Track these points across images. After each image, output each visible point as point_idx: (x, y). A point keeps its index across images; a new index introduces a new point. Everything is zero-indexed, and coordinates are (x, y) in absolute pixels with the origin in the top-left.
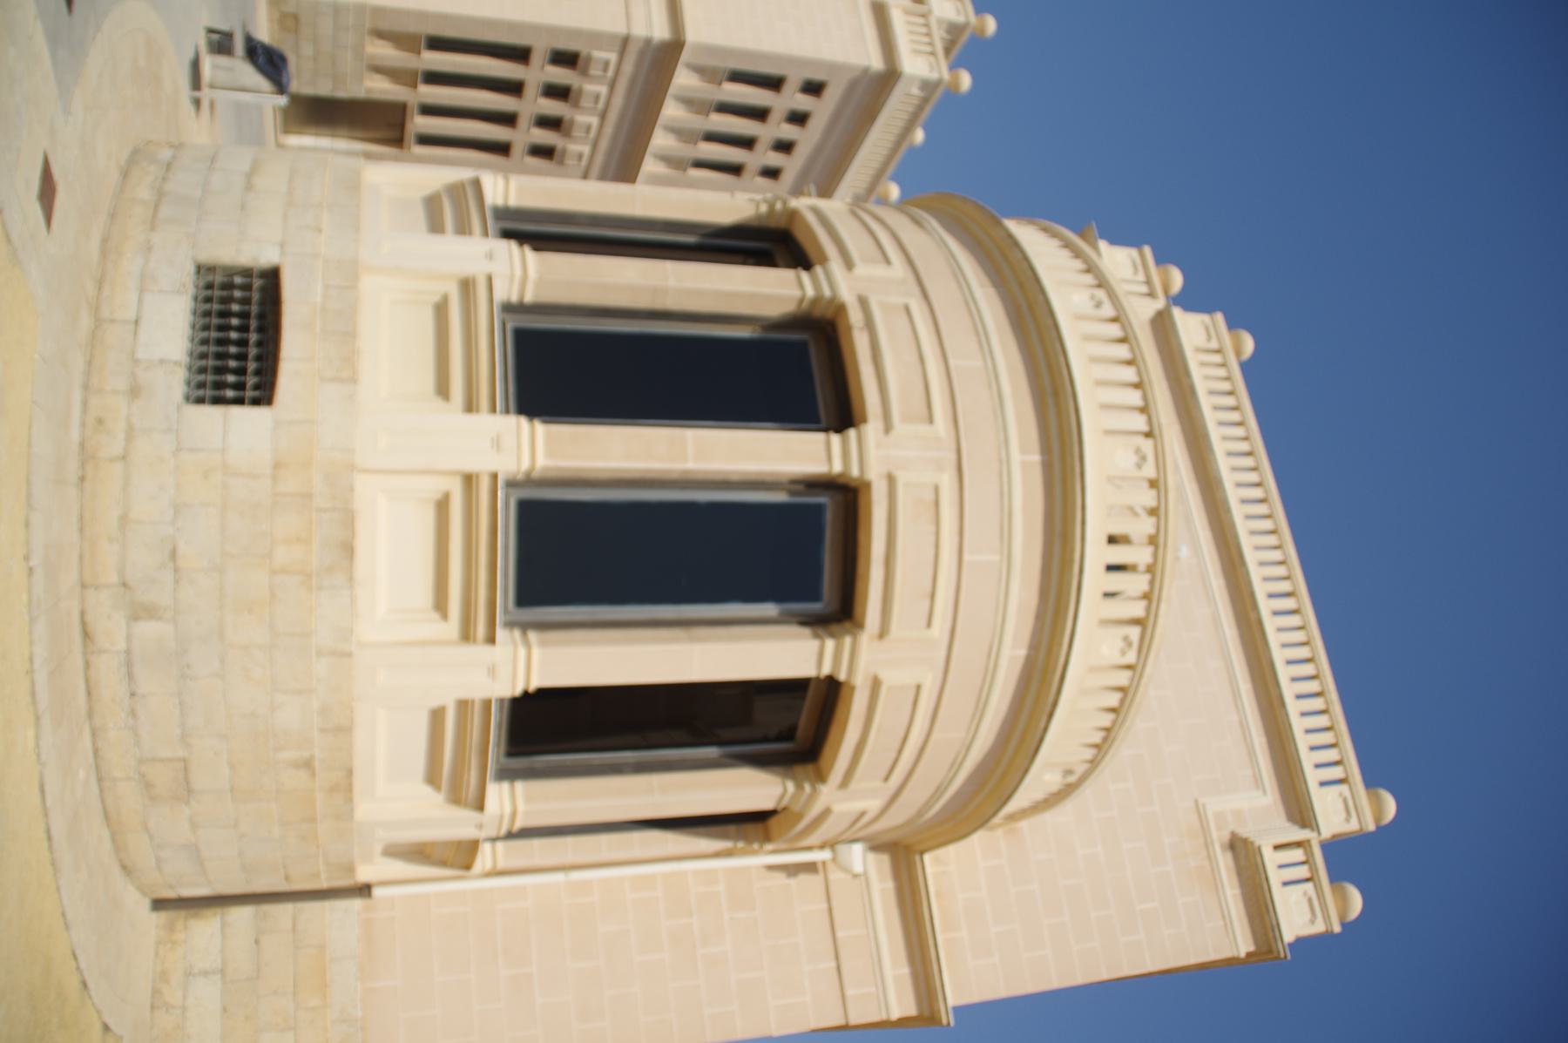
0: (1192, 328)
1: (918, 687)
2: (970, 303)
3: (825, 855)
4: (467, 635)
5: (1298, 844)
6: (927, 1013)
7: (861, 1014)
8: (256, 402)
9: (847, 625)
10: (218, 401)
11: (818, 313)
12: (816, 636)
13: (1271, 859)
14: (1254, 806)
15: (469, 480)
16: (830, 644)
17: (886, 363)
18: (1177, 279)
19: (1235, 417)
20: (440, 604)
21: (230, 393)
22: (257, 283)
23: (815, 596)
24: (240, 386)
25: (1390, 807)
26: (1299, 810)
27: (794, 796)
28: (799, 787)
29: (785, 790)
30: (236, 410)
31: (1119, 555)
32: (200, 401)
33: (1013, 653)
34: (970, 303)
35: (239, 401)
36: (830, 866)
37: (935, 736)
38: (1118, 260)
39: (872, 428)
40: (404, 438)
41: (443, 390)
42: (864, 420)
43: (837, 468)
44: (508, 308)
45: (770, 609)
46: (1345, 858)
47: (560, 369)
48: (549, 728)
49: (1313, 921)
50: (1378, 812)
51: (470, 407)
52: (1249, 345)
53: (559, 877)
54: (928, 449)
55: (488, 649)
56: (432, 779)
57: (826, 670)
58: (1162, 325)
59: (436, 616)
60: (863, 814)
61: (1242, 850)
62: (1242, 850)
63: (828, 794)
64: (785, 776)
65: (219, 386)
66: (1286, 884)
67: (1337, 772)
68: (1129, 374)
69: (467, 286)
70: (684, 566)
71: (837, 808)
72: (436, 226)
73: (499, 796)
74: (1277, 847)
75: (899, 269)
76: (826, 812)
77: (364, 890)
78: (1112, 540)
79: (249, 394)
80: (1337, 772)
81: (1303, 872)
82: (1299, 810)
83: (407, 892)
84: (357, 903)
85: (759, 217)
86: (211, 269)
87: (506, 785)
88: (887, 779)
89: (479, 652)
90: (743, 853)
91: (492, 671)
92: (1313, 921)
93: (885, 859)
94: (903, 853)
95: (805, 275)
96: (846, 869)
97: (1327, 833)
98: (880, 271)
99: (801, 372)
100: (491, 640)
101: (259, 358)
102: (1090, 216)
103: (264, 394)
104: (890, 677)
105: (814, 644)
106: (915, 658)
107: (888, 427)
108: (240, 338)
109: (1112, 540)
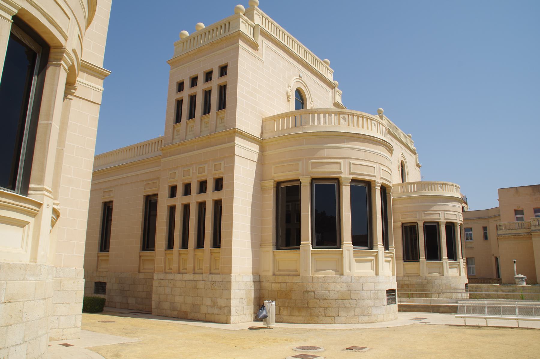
9: (52, 50)
20: (22, 224)
57: (10, 18)
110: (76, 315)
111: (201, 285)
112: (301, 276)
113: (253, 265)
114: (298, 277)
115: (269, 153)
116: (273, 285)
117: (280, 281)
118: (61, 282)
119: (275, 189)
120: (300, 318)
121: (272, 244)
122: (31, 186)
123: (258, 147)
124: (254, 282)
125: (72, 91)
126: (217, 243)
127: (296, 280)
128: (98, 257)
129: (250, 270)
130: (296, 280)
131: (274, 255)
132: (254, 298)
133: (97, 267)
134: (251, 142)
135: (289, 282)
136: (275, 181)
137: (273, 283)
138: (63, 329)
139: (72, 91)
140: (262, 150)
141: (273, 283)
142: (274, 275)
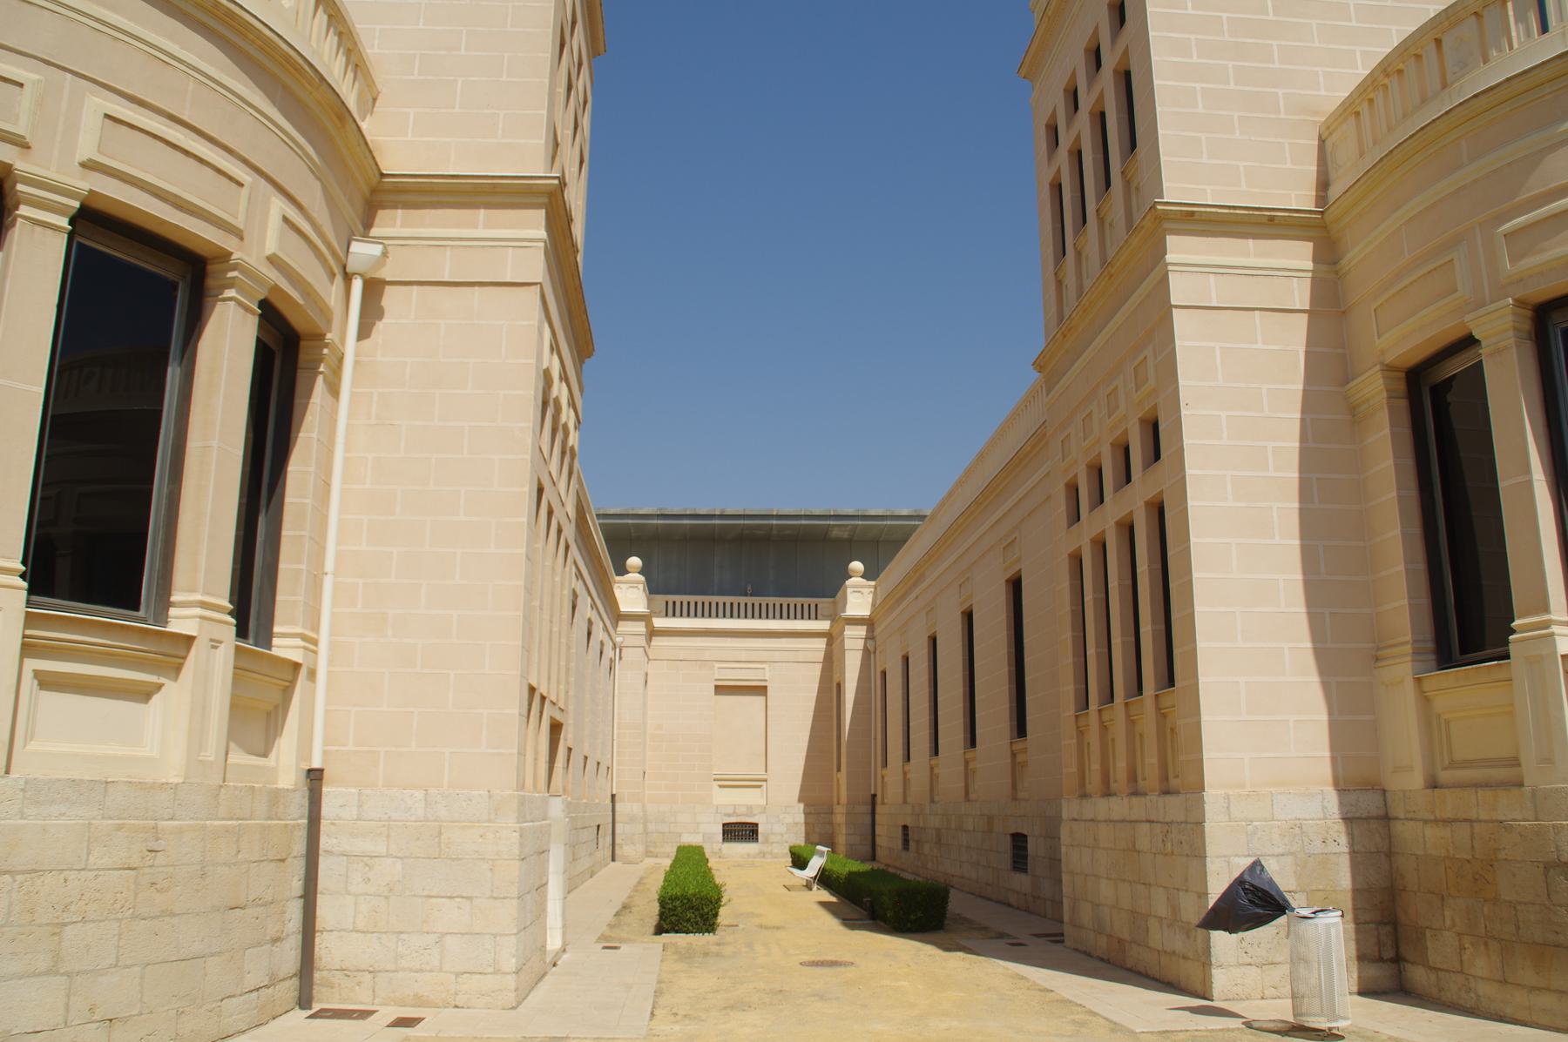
1: (107, 116)
6: (545, 200)
15: (29, 649)
16: (24, 210)
27: (241, 291)
28: (231, 284)
29: (230, 299)
56: (144, 694)
57: (64, 222)
59: (156, 698)
60: (286, 220)
71: (271, 247)
73: (181, 621)
77: (315, 777)
83: (311, 730)
87: (275, 641)
90: (337, 370)
93: (382, 215)
94: (377, 195)
104: (86, 149)
110: (495, 936)
111: (1143, 834)
112: (1527, 789)
113: (1333, 747)
114: (1515, 791)
115: (1354, 255)
116: (1429, 831)
117: (1449, 814)
118: (440, 834)
119: (1403, 404)
120: (1548, 1000)
121: (1408, 648)
122: (276, 629)
123: (1307, 248)
124: (1348, 820)
125: (230, 274)
126: (1169, 678)
127: (1508, 808)
128: (1014, 755)
129: (1326, 770)
130: (1508, 808)
131: (1425, 700)
132: (1356, 891)
133: (1014, 787)
134: (1256, 237)
135: (1482, 817)
136: (1389, 368)
137: (1426, 822)
138: (457, 975)
139: (230, 274)
140: (1329, 254)
141: (1426, 822)
142: (1433, 784)
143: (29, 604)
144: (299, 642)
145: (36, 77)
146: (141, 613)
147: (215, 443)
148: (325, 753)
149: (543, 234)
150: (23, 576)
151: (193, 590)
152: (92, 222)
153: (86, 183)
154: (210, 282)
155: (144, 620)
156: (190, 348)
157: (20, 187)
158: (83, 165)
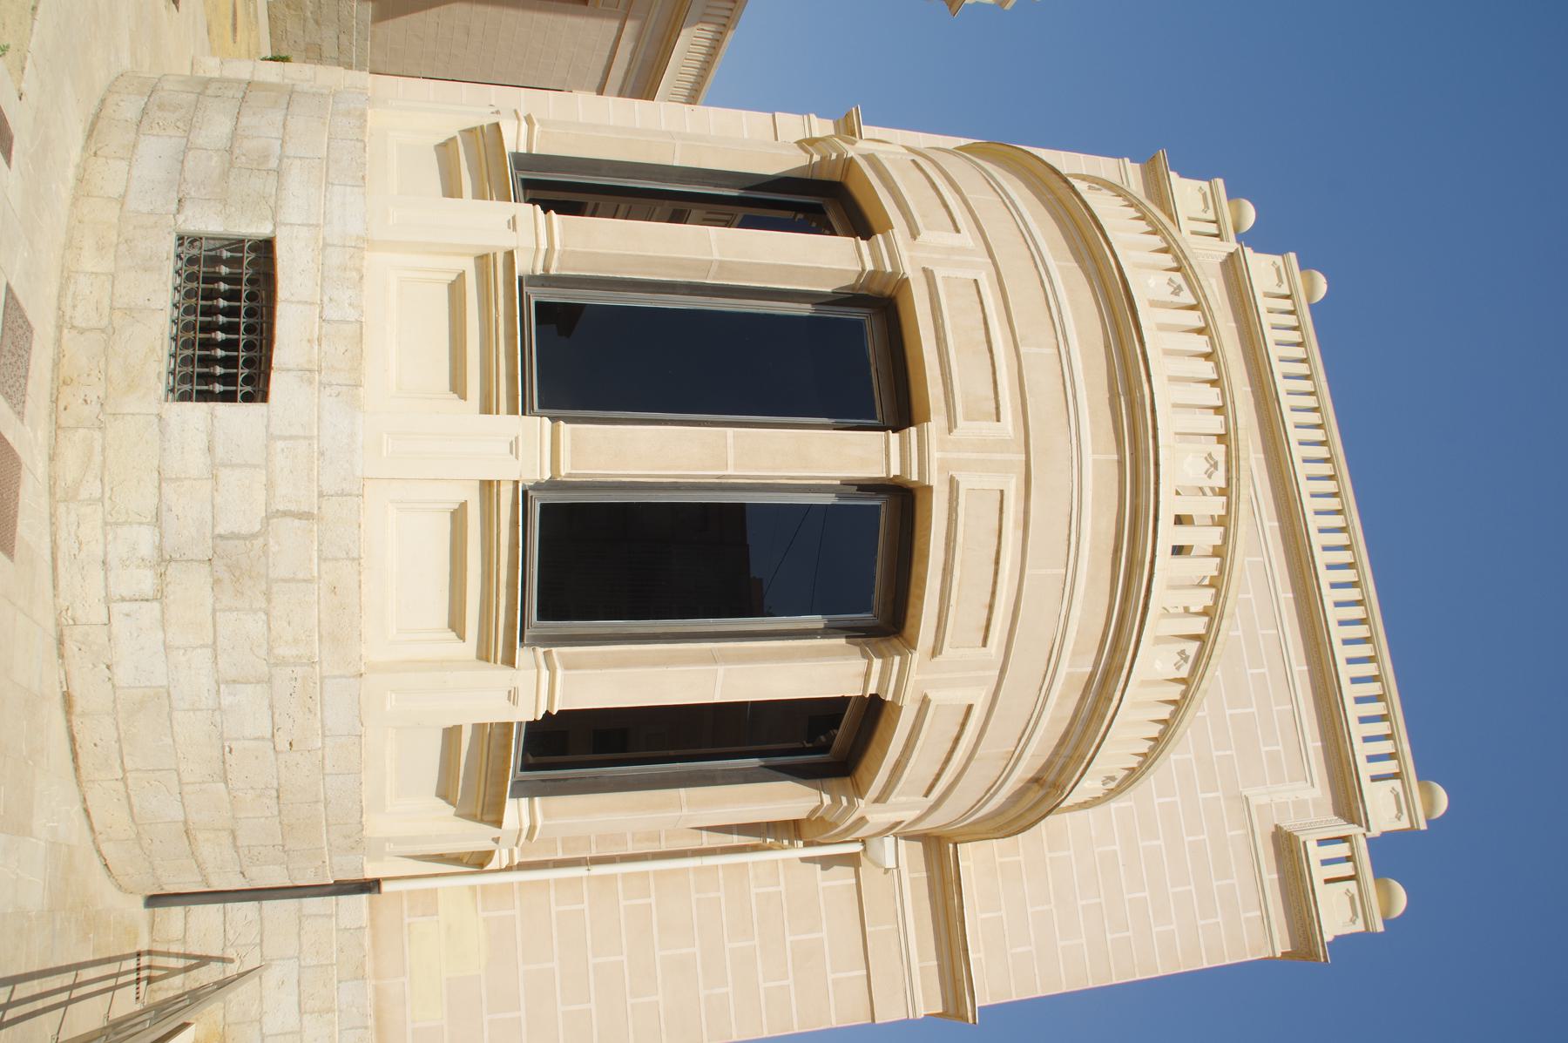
0: (1263, 270)
1: (970, 707)
2: (1009, 204)
3: (857, 848)
4: (484, 655)
5: (1344, 839)
7: (890, 1012)
8: (248, 398)
9: (895, 641)
10: (205, 396)
11: (876, 287)
12: (864, 655)
13: (1316, 853)
14: (1303, 800)
16: (877, 663)
17: (951, 348)
18: (1250, 215)
19: (1303, 369)
20: (456, 624)
21: (218, 388)
22: (248, 257)
23: (867, 608)
24: (228, 379)
25: (1442, 801)
26: (1347, 803)
30: (222, 408)
31: (1183, 536)
32: (185, 397)
33: (1076, 665)
34: (1009, 204)
35: (228, 397)
36: (863, 860)
37: (980, 751)
38: (1187, 193)
39: (935, 425)
40: (412, 444)
41: (457, 386)
42: (928, 419)
43: (895, 471)
44: (534, 280)
45: (816, 621)
46: (1390, 854)
47: (585, 352)
48: (569, 747)
49: (1353, 921)
50: (1430, 804)
51: (487, 408)
52: (1322, 286)
53: (580, 872)
54: (991, 449)
55: (509, 671)
56: (444, 793)
57: (872, 690)
58: (1232, 269)
61: (1286, 847)
62: (1286, 847)
63: (863, 806)
64: (822, 789)
65: (207, 378)
66: (1327, 881)
67: (1390, 767)
68: (1201, 344)
69: (483, 261)
70: (716, 546)
72: (451, 189)
73: (516, 811)
74: (1321, 842)
75: (968, 238)
76: (862, 821)
77: (369, 886)
78: (1179, 520)
79: (242, 389)
80: (1390, 767)
81: (1346, 869)
82: (1347, 803)
84: (364, 898)
85: (812, 166)
86: (195, 240)
87: (524, 801)
88: (926, 795)
89: (499, 676)
91: (512, 696)
92: (1353, 921)
93: (919, 845)
94: (938, 848)
95: (863, 244)
96: (877, 864)
97: (1375, 832)
98: (948, 238)
99: (854, 359)
100: (510, 661)
101: (250, 329)
102: (1165, 139)
103: (257, 391)
105: (859, 664)
106: (964, 675)
107: (951, 425)
108: (227, 328)
109: (1179, 520)
125: (844, 799)
139: (844, 799)
143: (520, 724)
144: (526, 825)
145: (1010, 428)
146: (520, 774)
147: (685, 811)
148: (399, 894)
149: (921, 1013)
150: (547, 714)
151: (546, 815)
152: (901, 502)
153: (936, 480)
154: (833, 783)
155: (514, 775)
156: (773, 773)
157: (897, 659)
158: (952, 479)
